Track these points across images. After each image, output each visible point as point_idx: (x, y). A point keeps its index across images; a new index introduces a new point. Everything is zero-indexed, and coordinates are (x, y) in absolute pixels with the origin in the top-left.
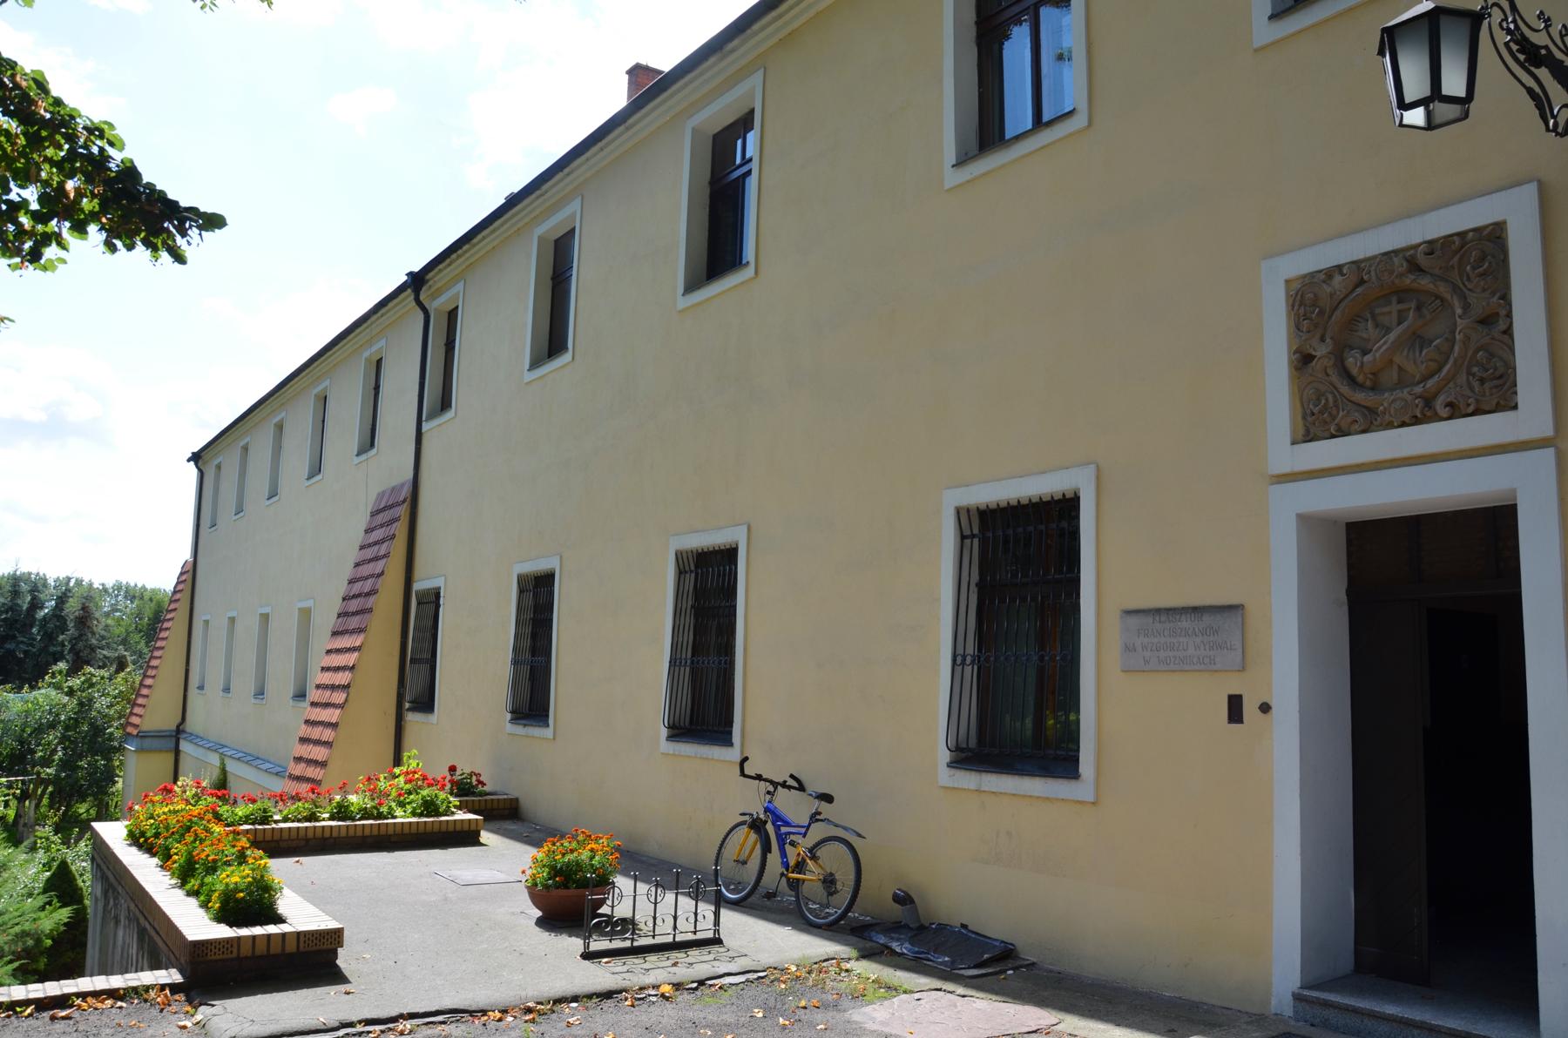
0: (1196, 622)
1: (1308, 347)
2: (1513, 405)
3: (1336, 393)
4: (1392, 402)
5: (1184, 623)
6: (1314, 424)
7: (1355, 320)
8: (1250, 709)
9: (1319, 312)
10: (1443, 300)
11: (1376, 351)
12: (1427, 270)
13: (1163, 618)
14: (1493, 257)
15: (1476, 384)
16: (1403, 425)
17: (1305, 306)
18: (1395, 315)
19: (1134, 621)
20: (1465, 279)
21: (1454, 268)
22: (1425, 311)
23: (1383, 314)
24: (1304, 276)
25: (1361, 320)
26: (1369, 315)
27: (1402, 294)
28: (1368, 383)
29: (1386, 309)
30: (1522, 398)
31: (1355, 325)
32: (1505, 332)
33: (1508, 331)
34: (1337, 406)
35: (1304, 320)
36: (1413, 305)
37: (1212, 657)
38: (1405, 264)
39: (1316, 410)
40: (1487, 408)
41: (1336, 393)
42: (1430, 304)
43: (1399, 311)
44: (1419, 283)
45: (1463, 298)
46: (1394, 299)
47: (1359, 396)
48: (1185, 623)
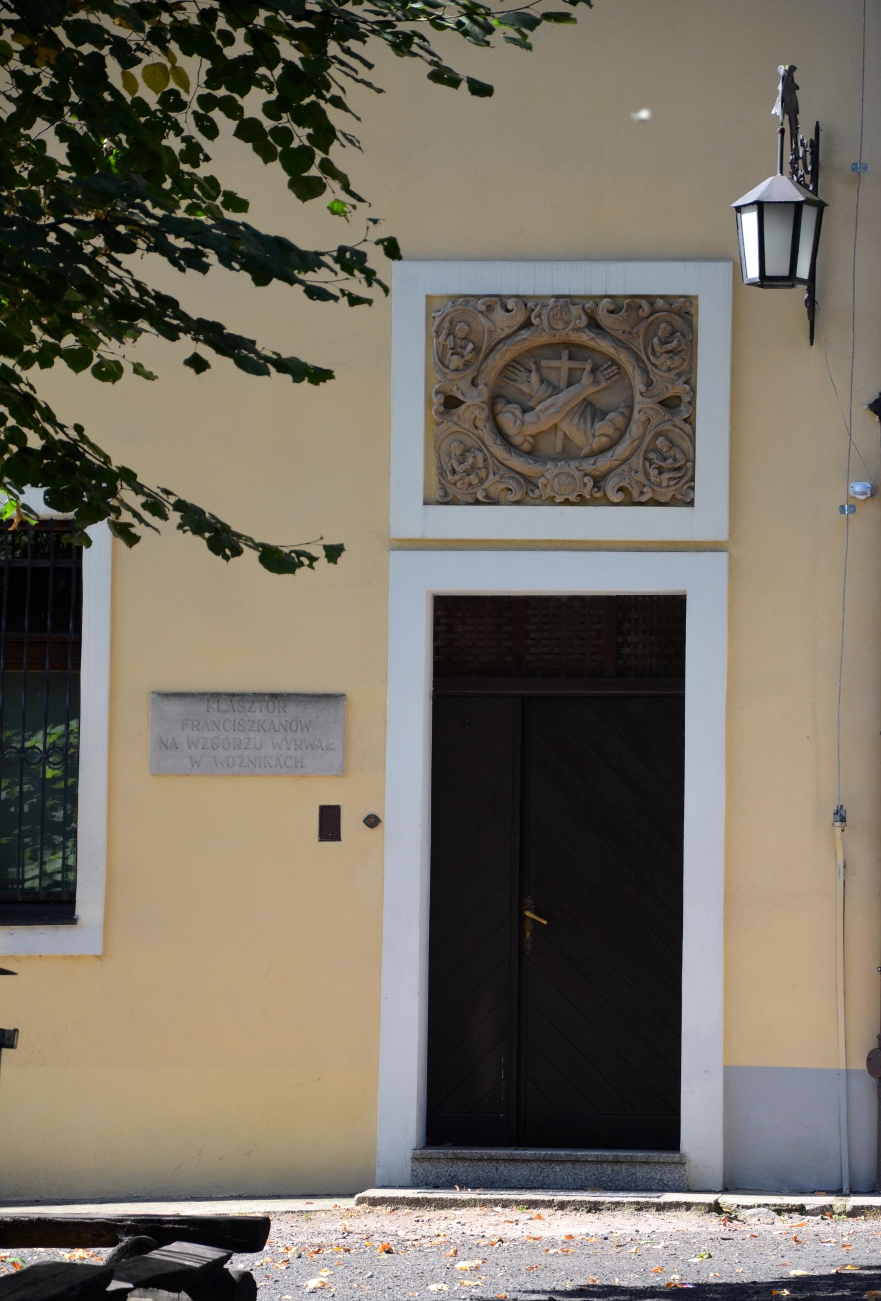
0: (276, 711)
1: (455, 388)
2: (689, 500)
3: (485, 451)
4: (556, 476)
5: (258, 713)
6: (455, 484)
7: (512, 366)
8: (350, 823)
9: (473, 350)
10: (620, 367)
11: (542, 411)
12: (607, 329)
13: (223, 706)
14: (683, 335)
15: (653, 473)
16: (567, 502)
17: (455, 336)
18: (564, 374)
19: (174, 708)
20: (649, 351)
21: (638, 336)
22: (599, 375)
23: (550, 368)
24: (454, 298)
25: (522, 369)
26: (533, 367)
27: (575, 351)
28: (526, 447)
29: (555, 364)
30: (699, 495)
31: (516, 375)
32: (685, 420)
33: (690, 421)
34: (486, 467)
35: (453, 354)
36: (588, 368)
37: (299, 759)
38: (584, 317)
39: (460, 469)
40: (662, 500)
41: (485, 451)
42: (605, 369)
43: (570, 369)
44: (597, 343)
45: (645, 371)
46: (565, 354)
47: (517, 463)
48: (259, 713)
